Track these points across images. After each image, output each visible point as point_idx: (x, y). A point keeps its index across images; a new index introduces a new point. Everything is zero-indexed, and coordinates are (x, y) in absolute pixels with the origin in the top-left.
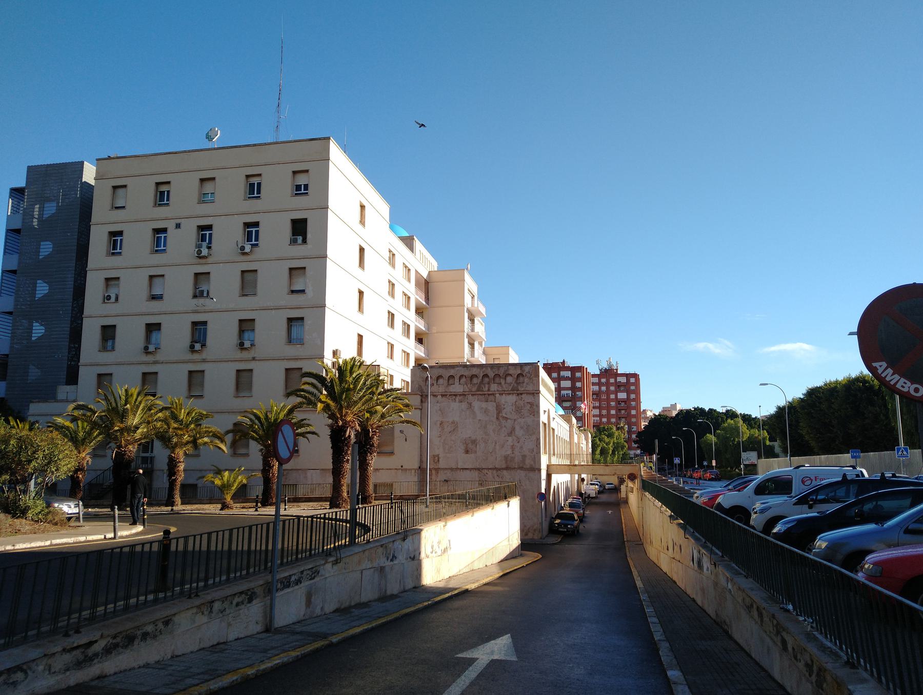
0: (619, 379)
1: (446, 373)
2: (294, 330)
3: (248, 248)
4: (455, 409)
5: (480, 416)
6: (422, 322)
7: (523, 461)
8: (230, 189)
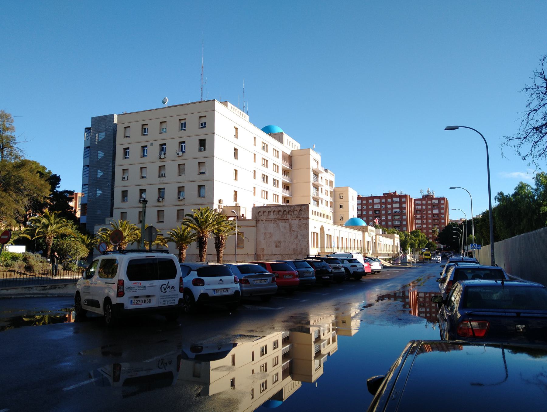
0: (434, 201)
1: (267, 210)
2: (202, 191)
3: (180, 154)
4: (271, 227)
5: (282, 230)
6: (288, 178)
7: (302, 251)
8: (173, 126)
